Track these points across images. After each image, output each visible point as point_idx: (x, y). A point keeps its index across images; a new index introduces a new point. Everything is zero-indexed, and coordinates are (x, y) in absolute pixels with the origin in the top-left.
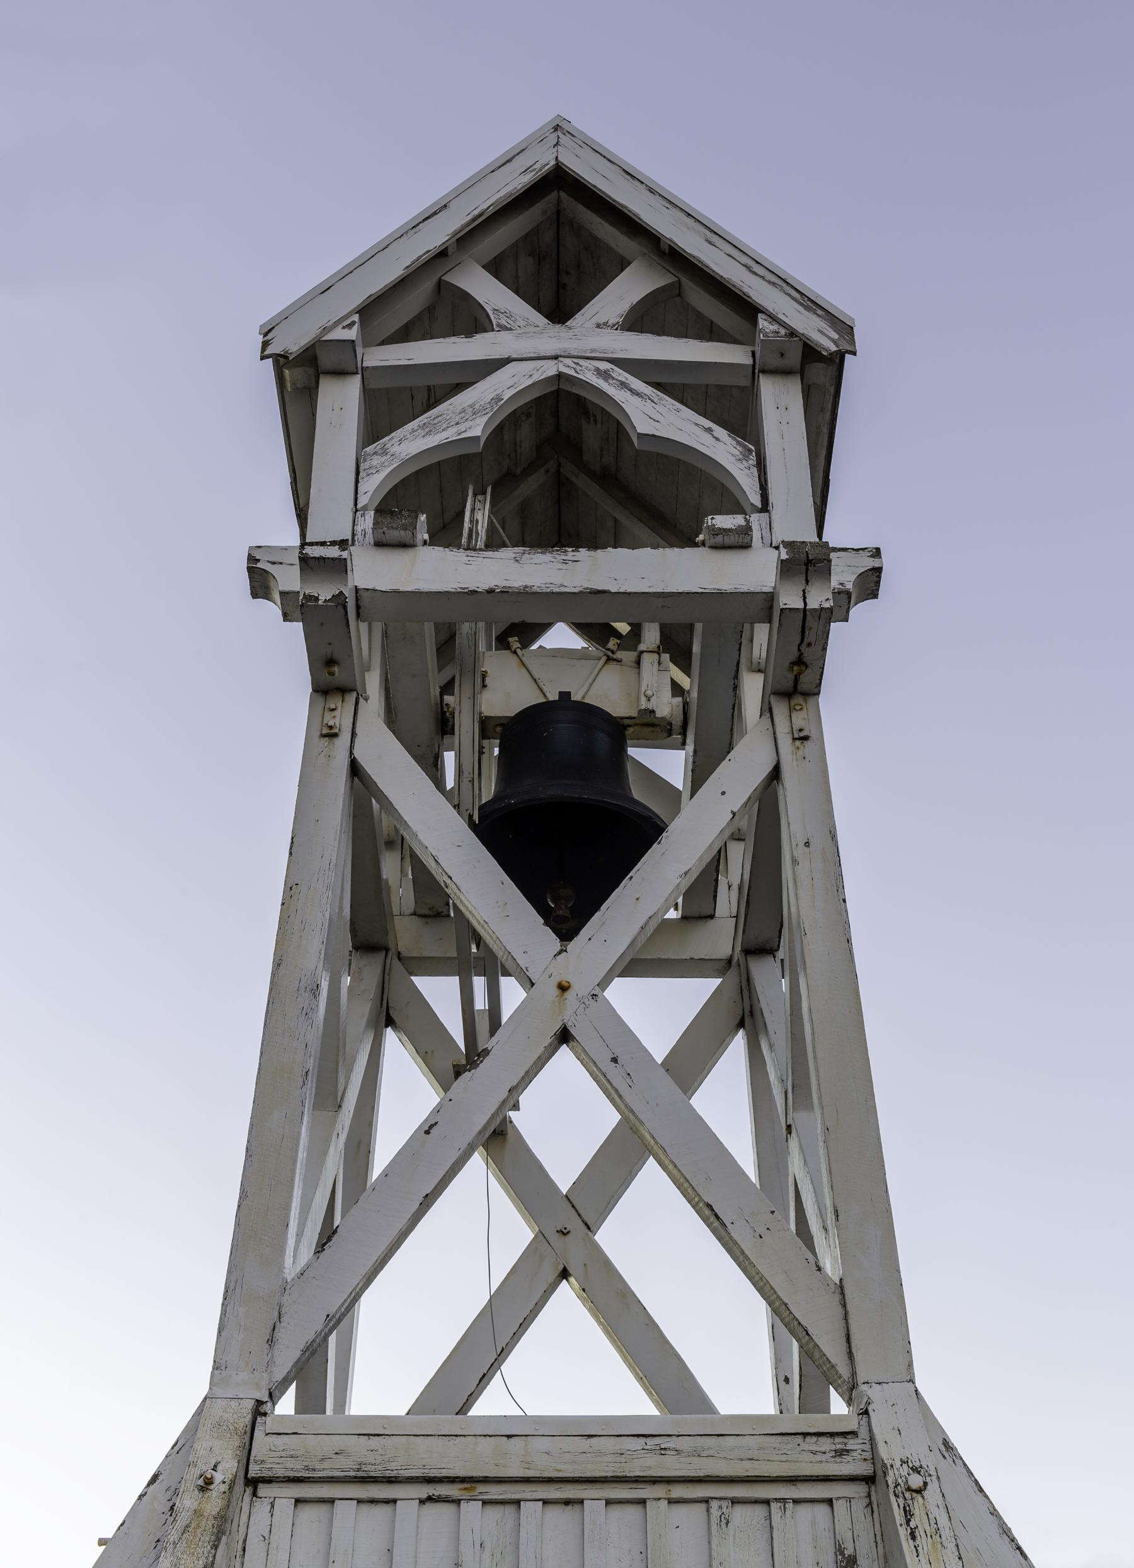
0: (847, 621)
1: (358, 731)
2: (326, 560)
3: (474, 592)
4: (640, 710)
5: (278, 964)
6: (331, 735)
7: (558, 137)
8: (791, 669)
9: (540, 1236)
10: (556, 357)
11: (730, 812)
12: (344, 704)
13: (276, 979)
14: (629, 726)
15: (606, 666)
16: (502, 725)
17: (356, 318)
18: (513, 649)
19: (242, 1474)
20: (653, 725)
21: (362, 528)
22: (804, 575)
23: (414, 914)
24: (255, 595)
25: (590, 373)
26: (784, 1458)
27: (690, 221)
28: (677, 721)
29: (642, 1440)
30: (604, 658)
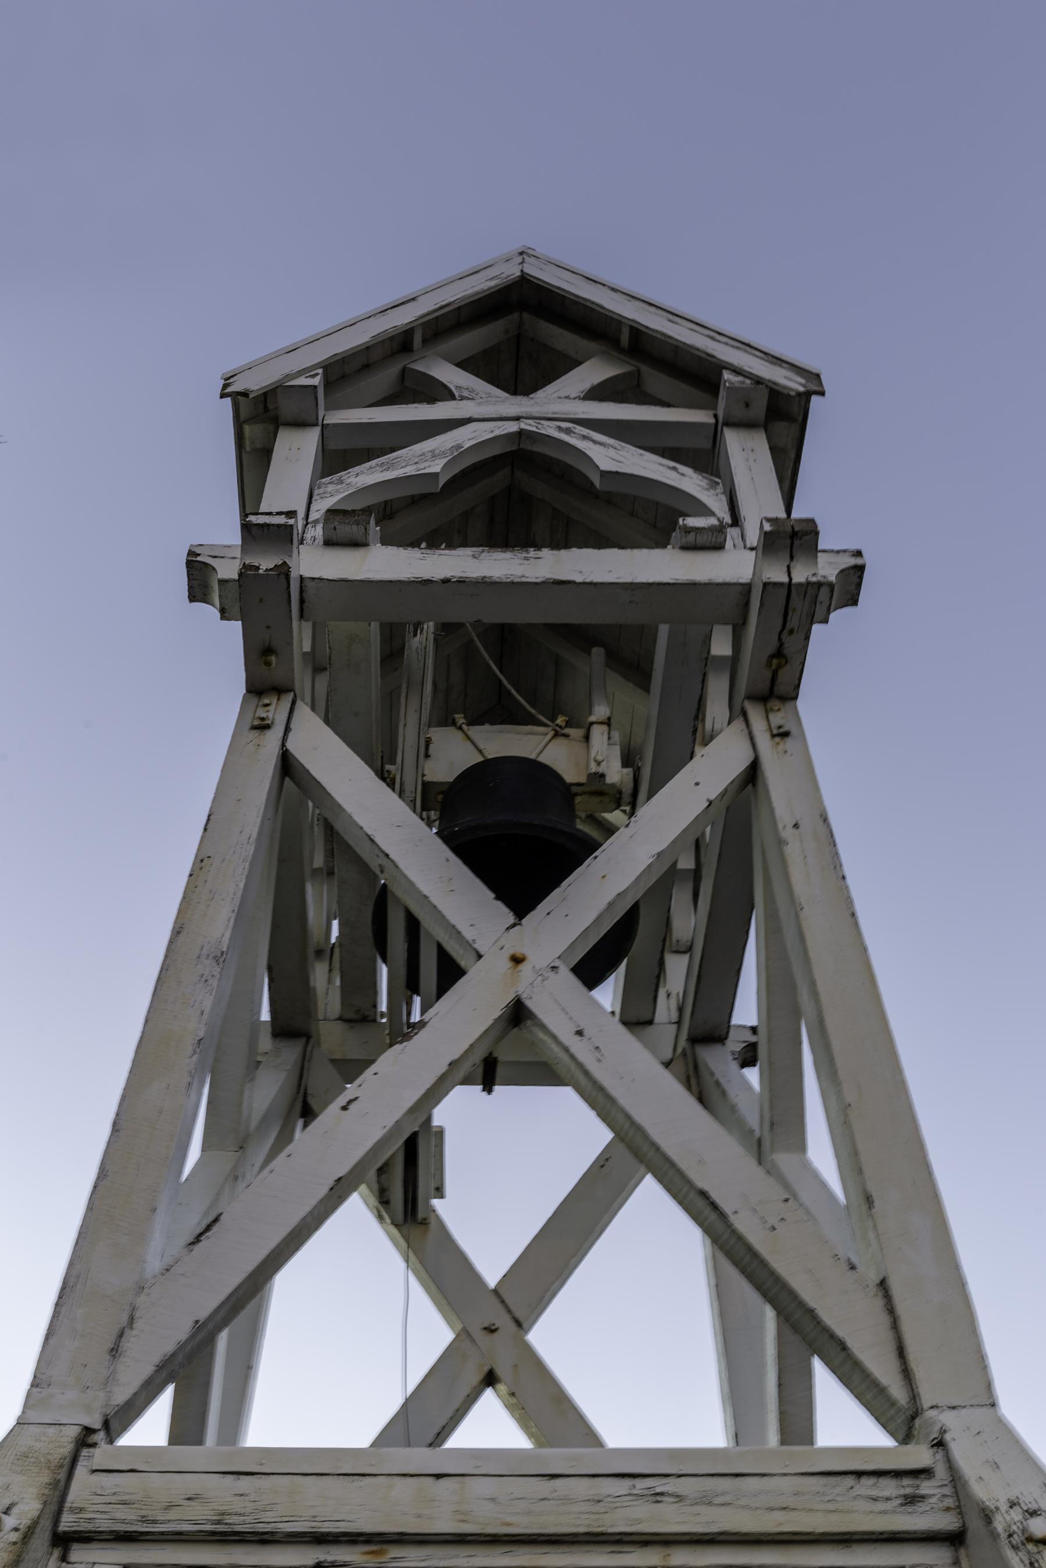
0: (827, 623)
1: (292, 726)
2: (271, 527)
4: (590, 774)
5: (177, 931)
6: (263, 727)
7: (523, 258)
8: (769, 663)
9: (463, 1336)
11: (705, 800)
12: (280, 702)
13: (173, 946)
14: (577, 794)
15: (554, 741)
16: (442, 793)
17: (320, 371)
18: (458, 725)
19: (46, 1524)
20: (601, 793)
21: (312, 535)
22: (789, 549)
23: (340, 1019)
24: (192, 598)
25: (552, 429)
26: (831, 1506)
28: (628, 787)
29: (627, 1483)
30: (552, 733)
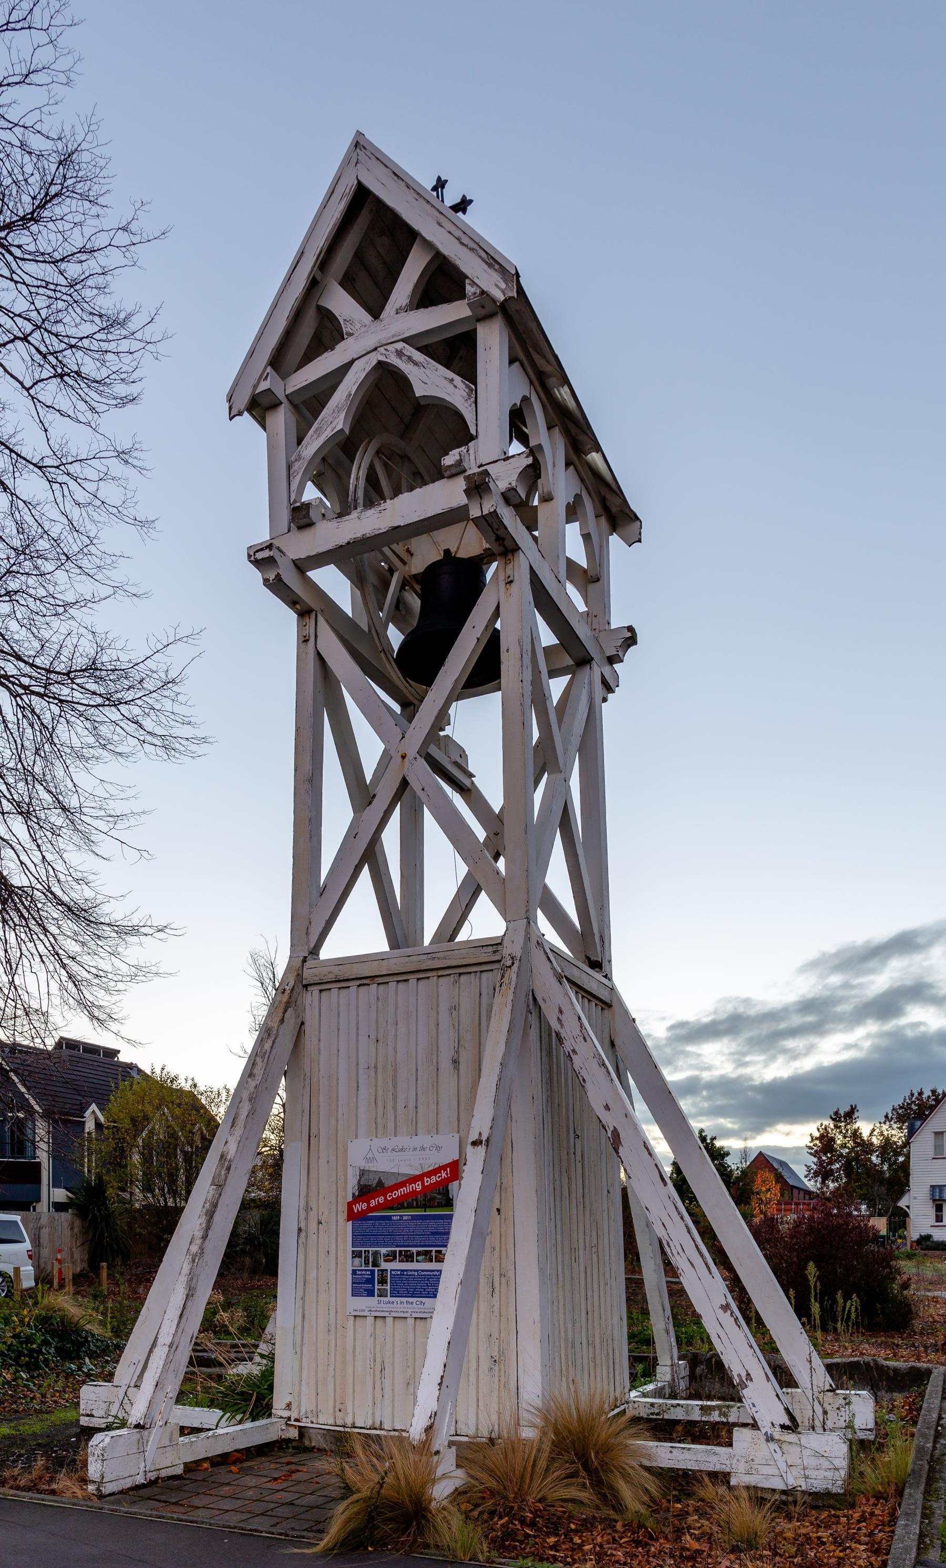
3: (341, 546)
10: (376, 349)
17: (269, 369)
27: (428, 207)
